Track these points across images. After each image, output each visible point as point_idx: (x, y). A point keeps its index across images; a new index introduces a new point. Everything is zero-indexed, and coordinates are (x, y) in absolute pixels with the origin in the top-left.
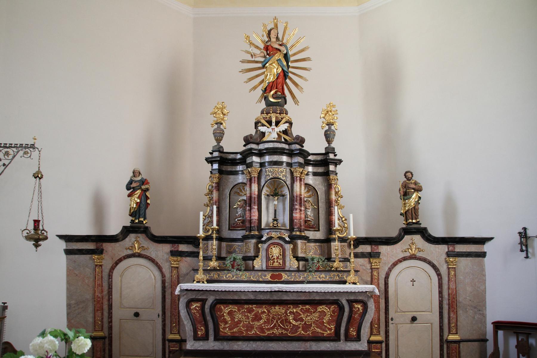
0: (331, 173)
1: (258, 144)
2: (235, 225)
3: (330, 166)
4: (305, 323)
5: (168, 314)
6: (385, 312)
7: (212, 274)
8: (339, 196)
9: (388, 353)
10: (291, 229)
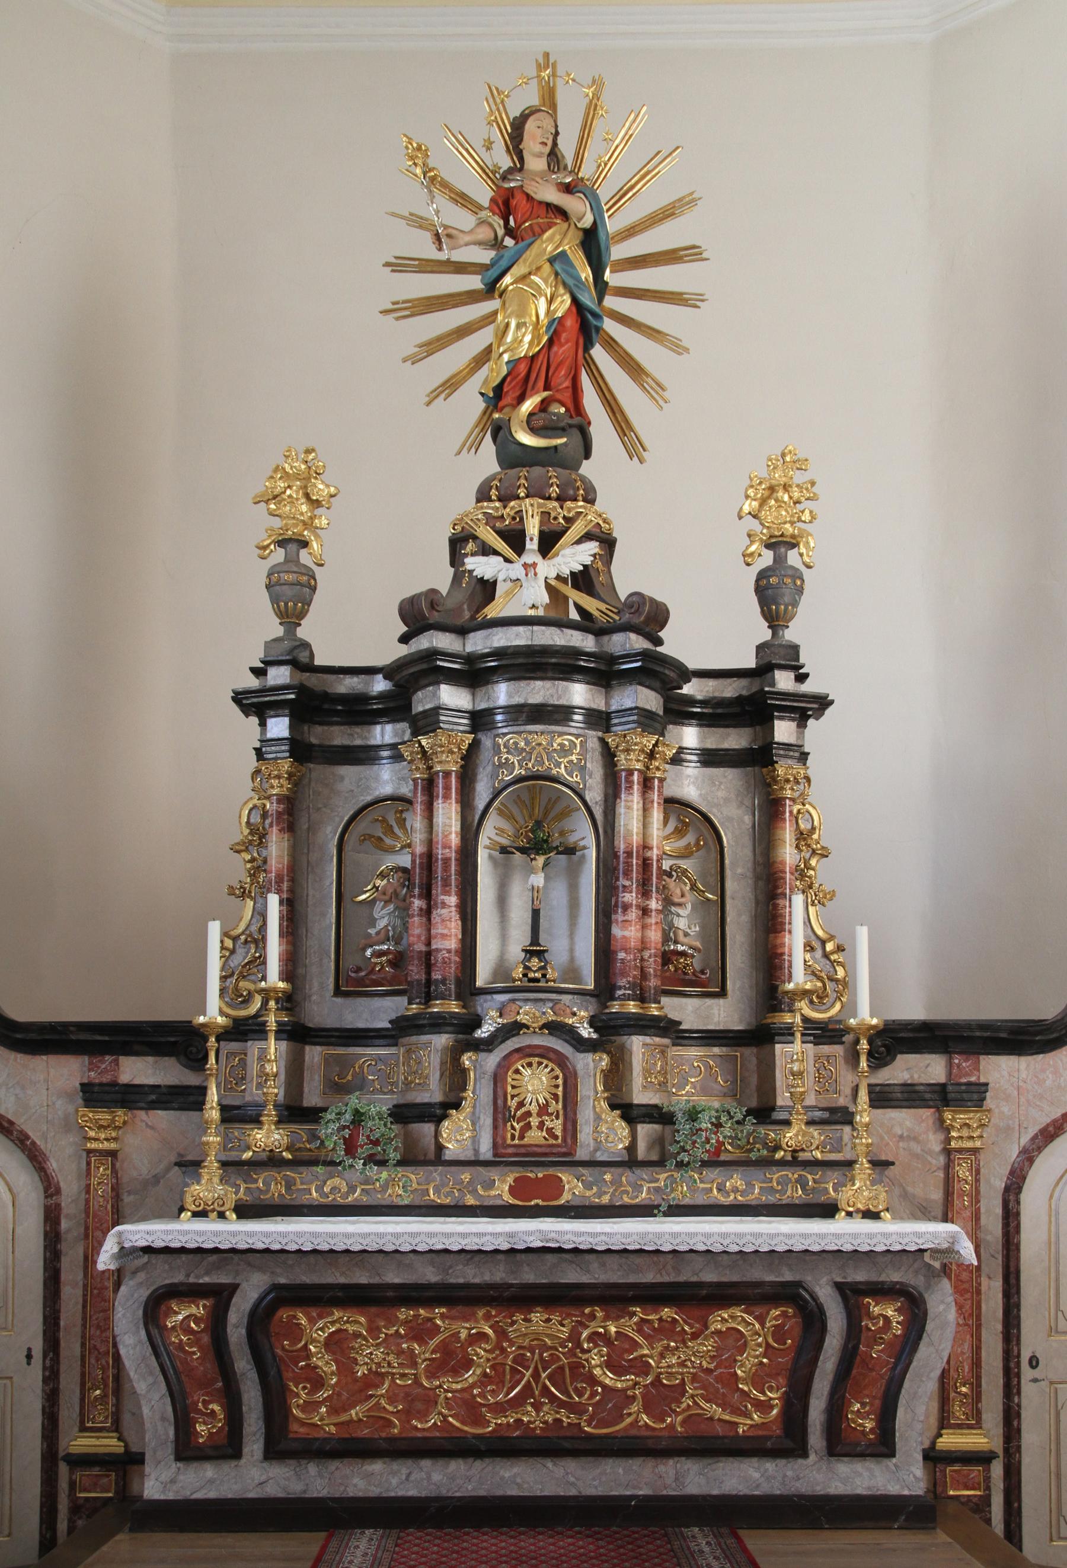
0: (782, 752)
1: (462, 631)
2: (363, 974)
3: (776, 722)
4: (657, 1380)
5: (71, 1347)
6: (1002, 1333)
7: (260, 1181)
8: (814, 852)
9: (1016, 1505)
10: (604, 990)
